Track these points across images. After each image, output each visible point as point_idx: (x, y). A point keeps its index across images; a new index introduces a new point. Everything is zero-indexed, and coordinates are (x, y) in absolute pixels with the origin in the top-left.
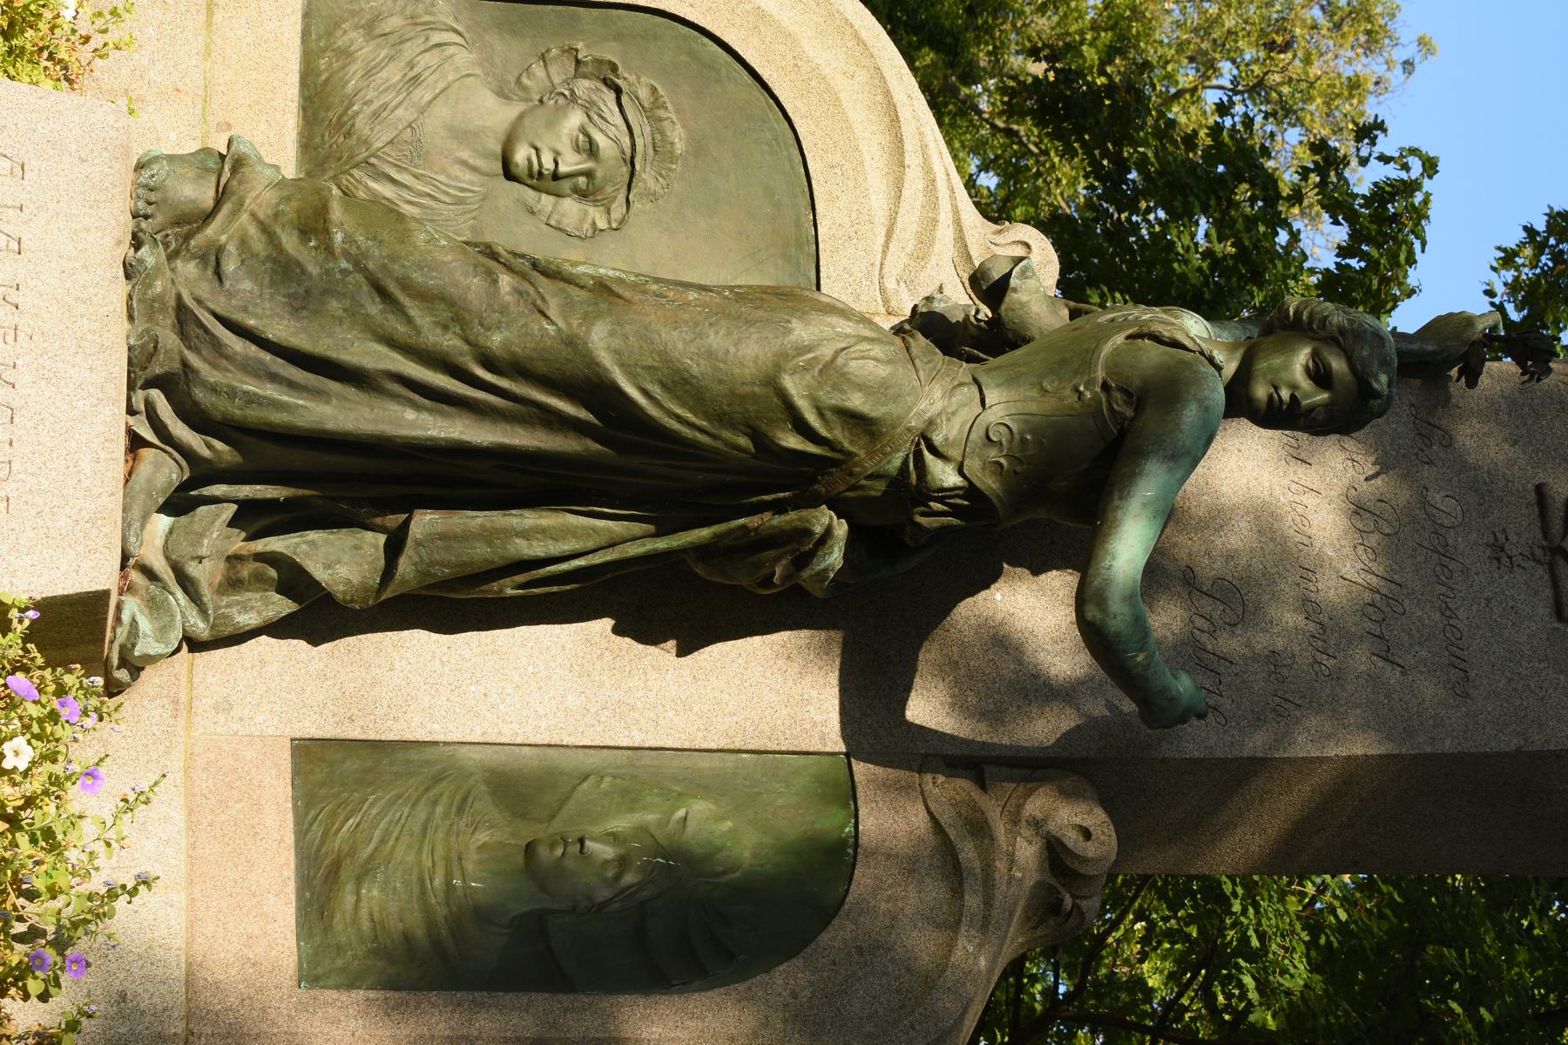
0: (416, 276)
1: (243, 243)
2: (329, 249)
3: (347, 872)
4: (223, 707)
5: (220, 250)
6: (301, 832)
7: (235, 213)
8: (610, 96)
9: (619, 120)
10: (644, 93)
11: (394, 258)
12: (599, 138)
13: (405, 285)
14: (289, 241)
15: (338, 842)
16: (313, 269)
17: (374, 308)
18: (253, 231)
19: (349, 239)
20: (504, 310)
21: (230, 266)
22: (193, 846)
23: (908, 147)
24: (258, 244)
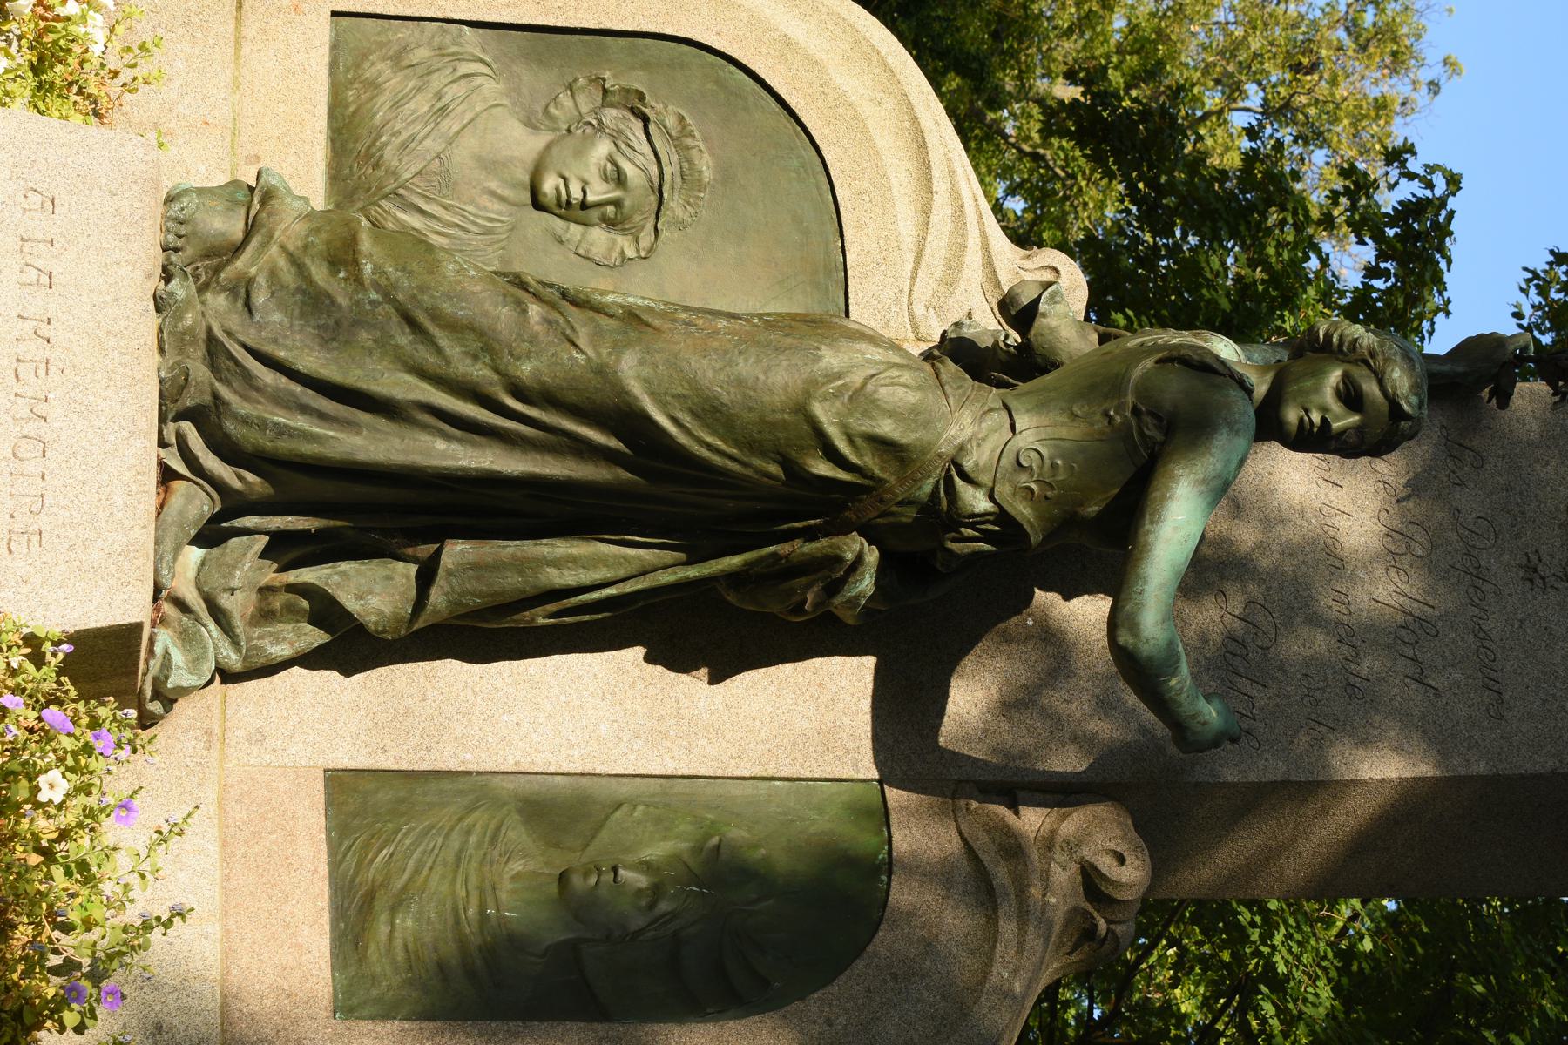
0: (446, 307)
1: (273, 274)
2: (358, 280)
3: (381, 902)
4: (257, 738)
5: (250, 283)
6: (335, 863)
7: (264, 245)
8: (638, 125)
9: (647, 149)
10: (671, 122)
11: (423, 289)
12: (627, 167)
13: (435, 315)
15: (372, 873)
16: (343, 301)
17: (404, 339)
18: (282, 262)
19: (378, 269)
20: (533, 339)
21: (260, 298)
22: (227, 878)
23: (936, 173)
24: (288, 276)
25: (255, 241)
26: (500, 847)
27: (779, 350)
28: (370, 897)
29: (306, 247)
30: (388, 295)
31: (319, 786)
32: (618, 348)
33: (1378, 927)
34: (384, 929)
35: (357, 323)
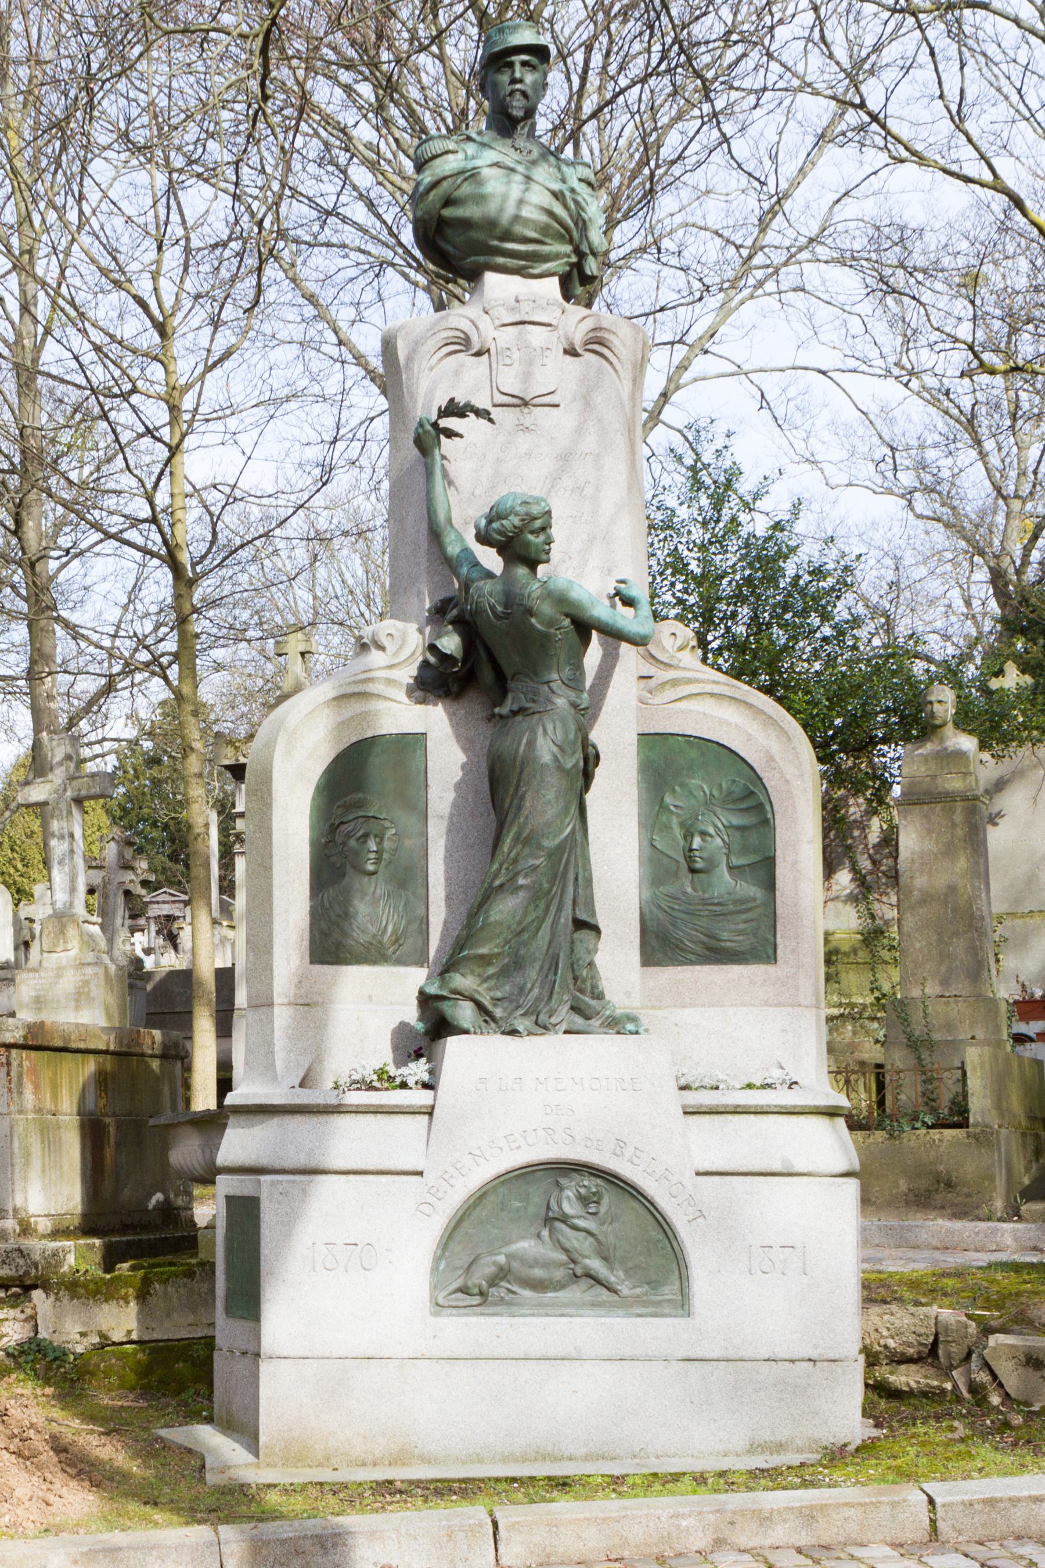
0: (518, 918)
1: (490, 989)
2: (498, 954)
3: (713, 943)
4: (628, 994)
5: (492, 999)
6: (692, 963)
7: (479, 993)
8: (343, 827)
9: (353, 823)
10: (339, 812)
11: (509, 927)
12: (360, 833)
13: (520, 923)
14: (491, 970)
15: (698, 949)
16: (506, 961)
17: (526, 936)
18: (485, 985)
19: (496, 946)
20: (534, 882)
21: (499, 994)
22: (703, 1006)
23: (356, 690)
24: (492, 983)
25: (477, 997)
26: (680, 896)
27: (543, 780)
28: (710, 949)
29: (479, 976)
30: (507, 942)
31: (652, 970)
32: (540, 847)
33: (14, 363)
34: (728, 944)
35: (516, 954)
